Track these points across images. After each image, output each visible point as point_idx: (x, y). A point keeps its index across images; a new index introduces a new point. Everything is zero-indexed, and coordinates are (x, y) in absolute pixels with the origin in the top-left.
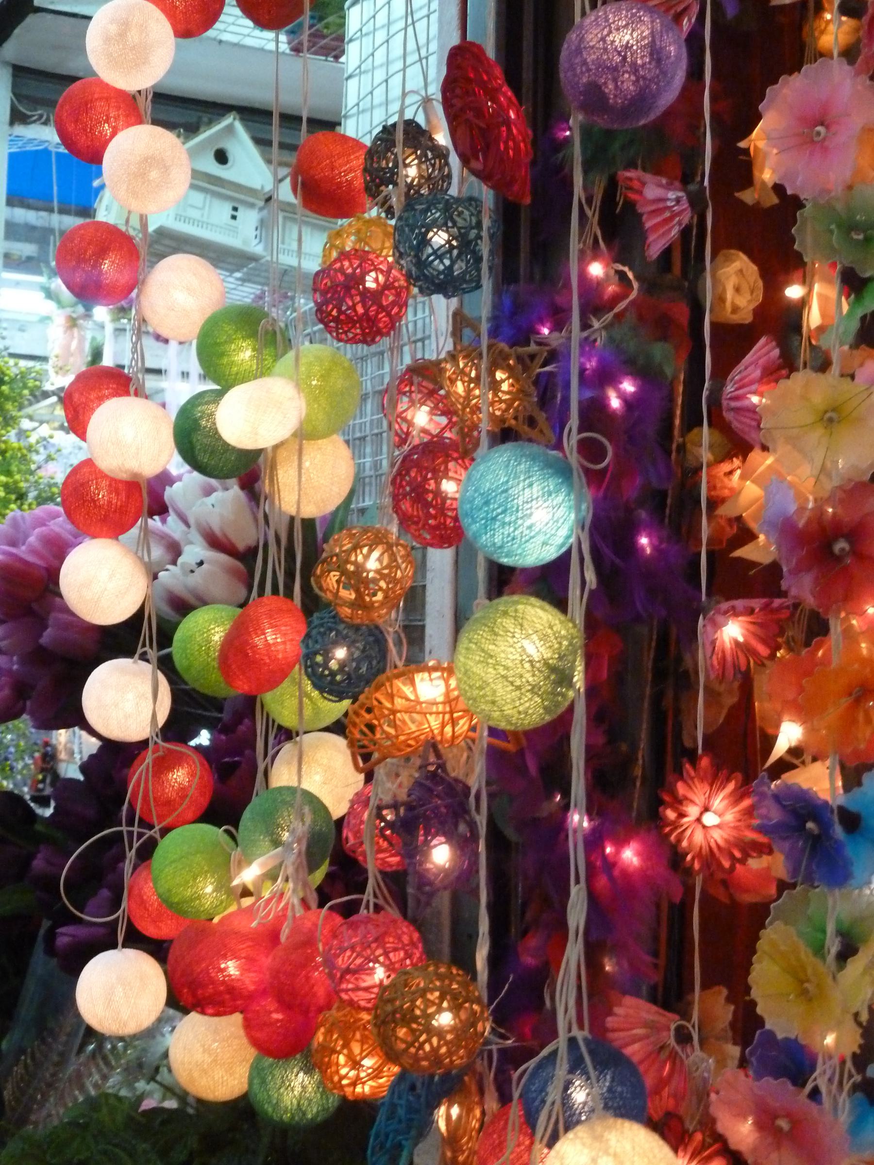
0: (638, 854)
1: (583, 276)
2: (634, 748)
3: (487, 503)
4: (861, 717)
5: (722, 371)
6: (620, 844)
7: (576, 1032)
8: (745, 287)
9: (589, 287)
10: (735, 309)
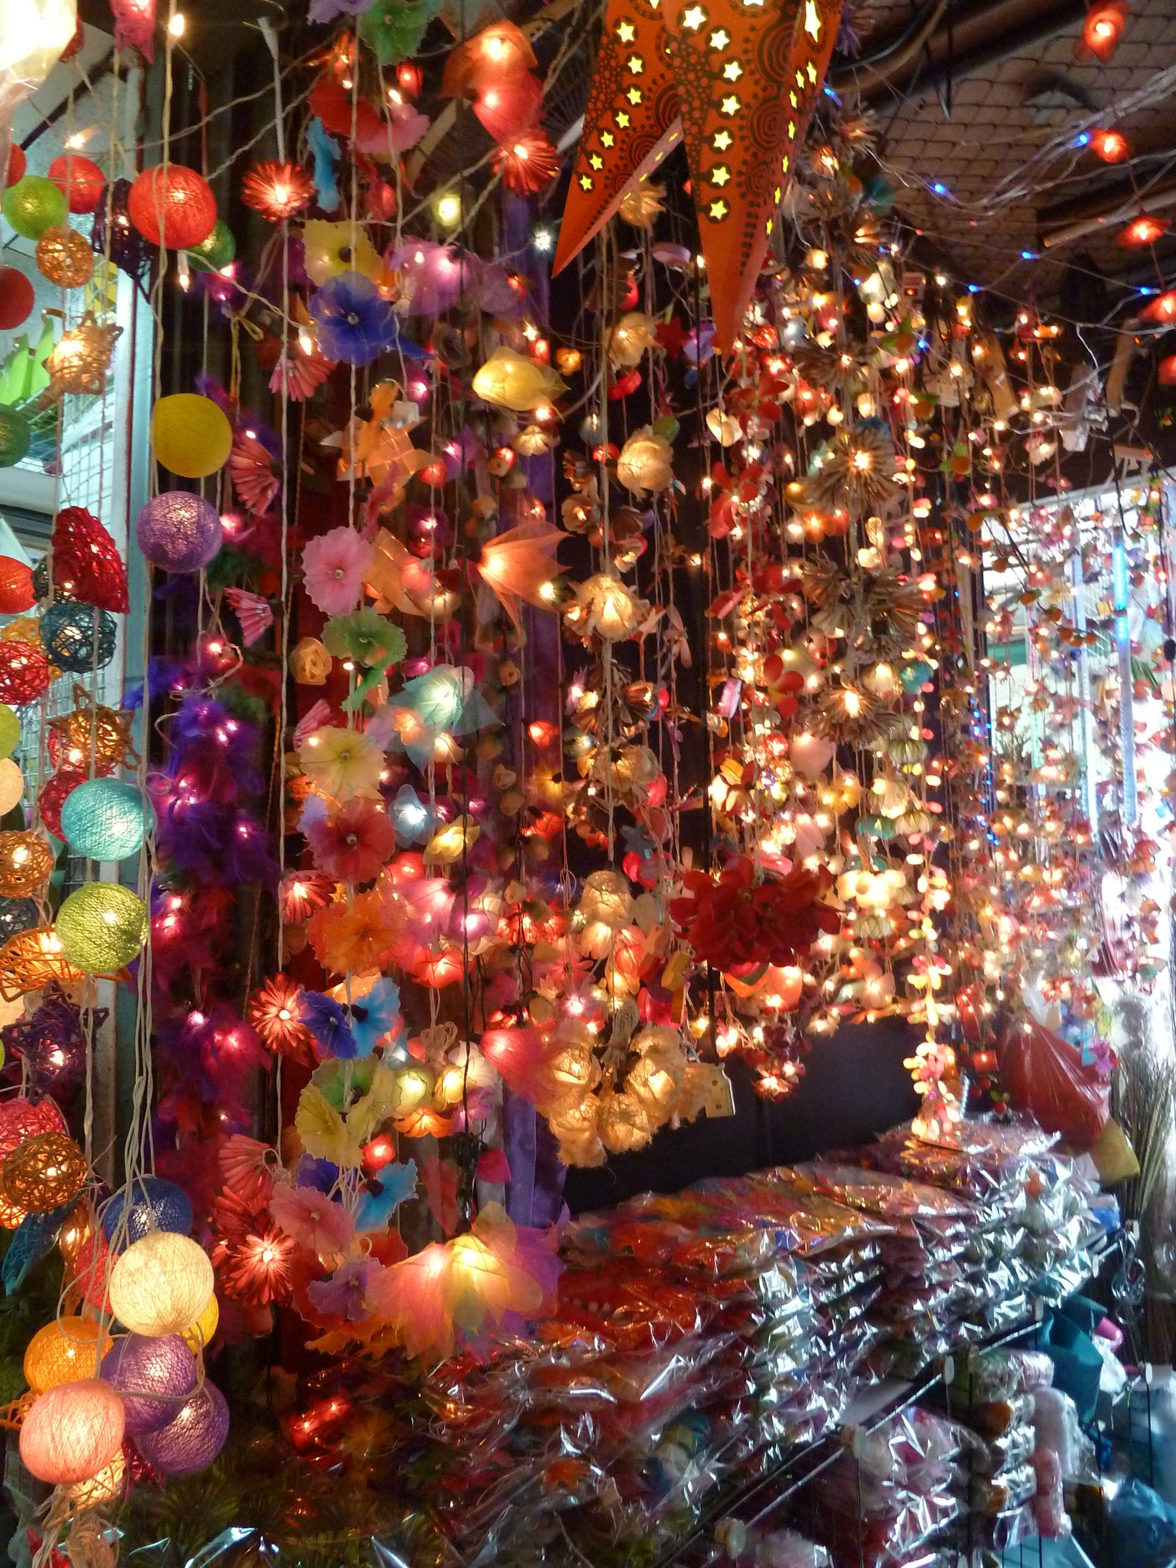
0: (237, 1040)
1: (204, 650)
2: (244, 967)
3: (80, 820)
4: (365, 949)
5: (293, 721)
6: (226, 1033)
7: (142, 1176)
8: (320, 663)
9: (210, 660)
10: (313, 676)
